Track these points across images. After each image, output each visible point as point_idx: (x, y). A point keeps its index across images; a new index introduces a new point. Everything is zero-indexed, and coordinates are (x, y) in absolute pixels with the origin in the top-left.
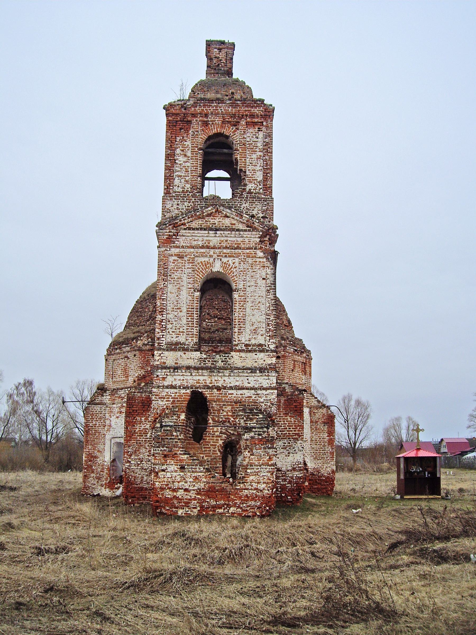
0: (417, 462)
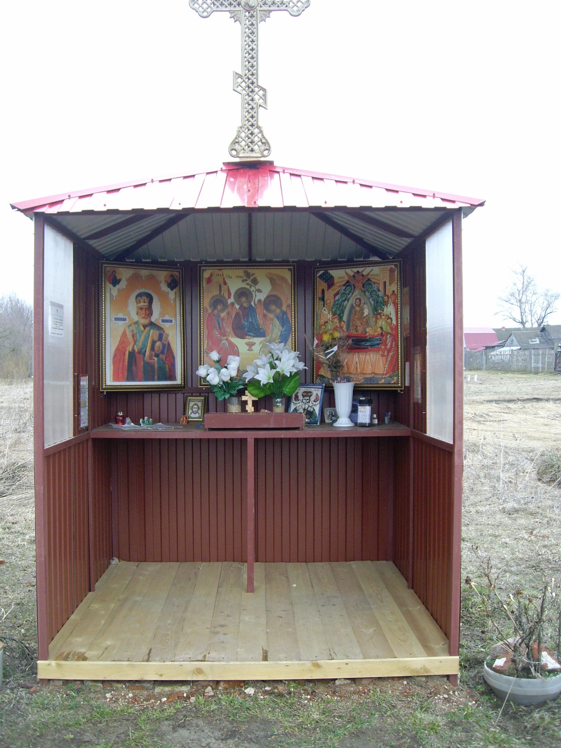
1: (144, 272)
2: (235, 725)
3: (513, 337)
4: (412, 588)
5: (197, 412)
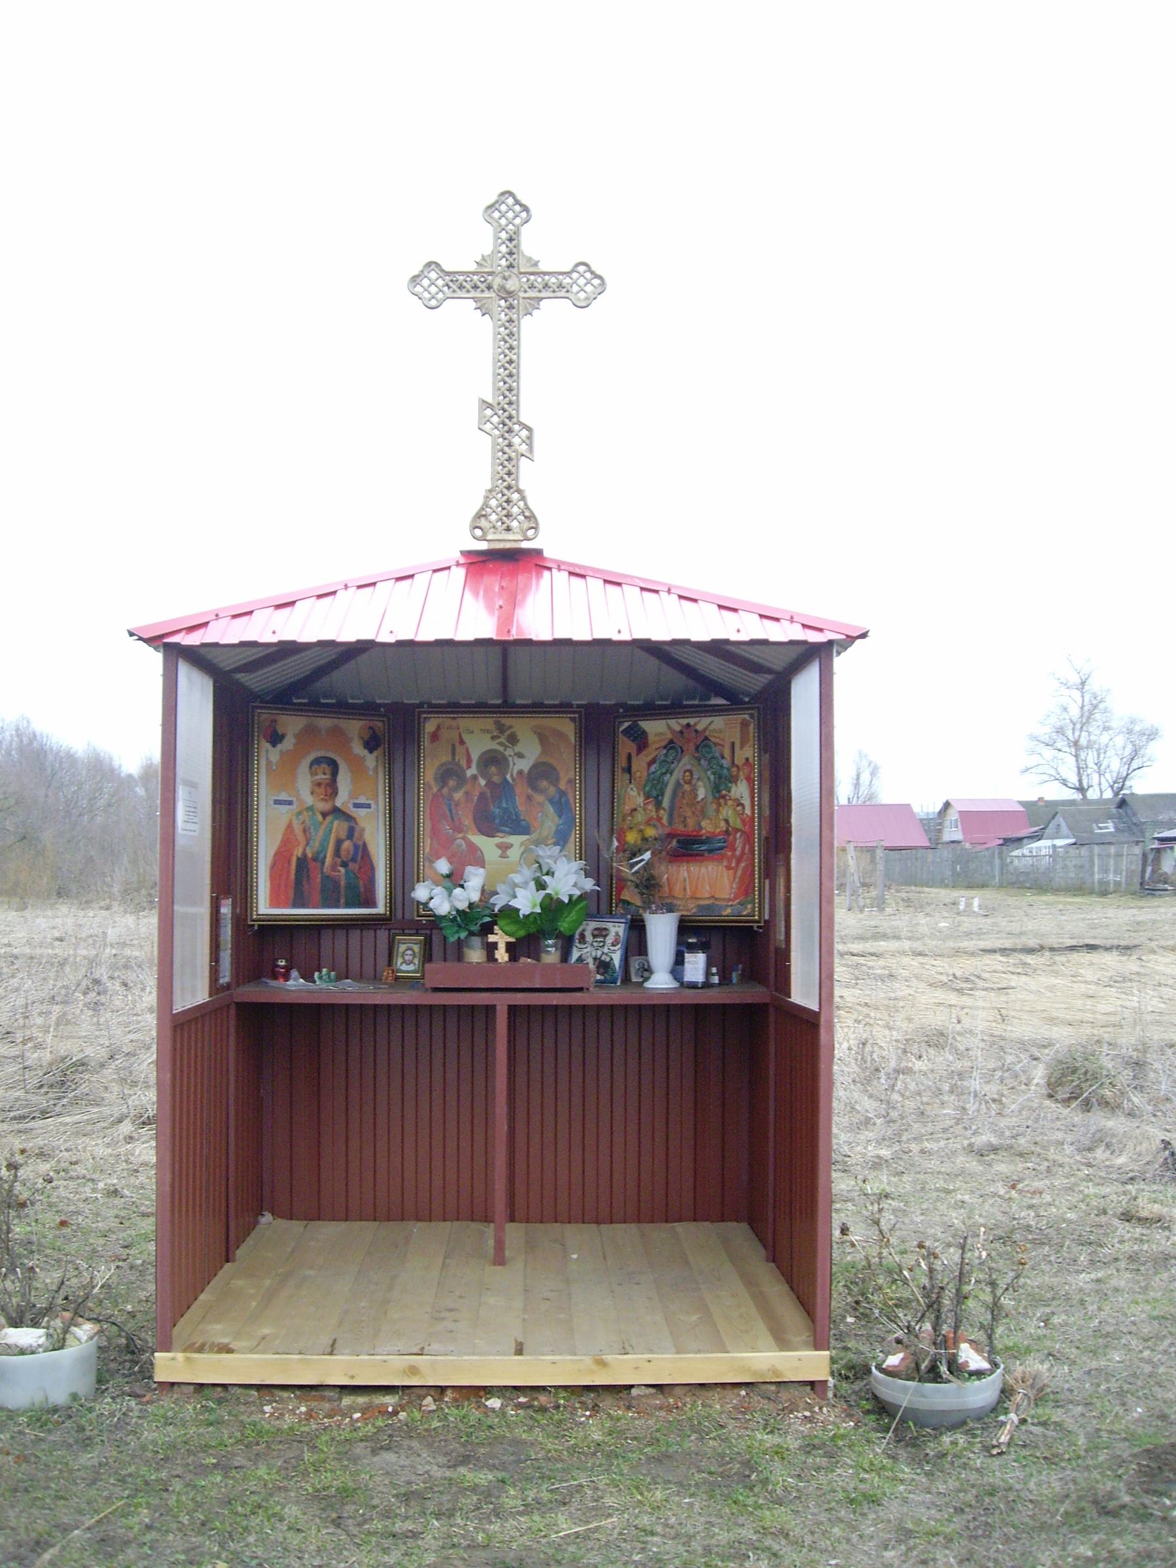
0: (542, 773)
1: (324, 723)
2: (469, 1447)
3: (1059, 819)
4: (774, 1261)
5: (411, 962)
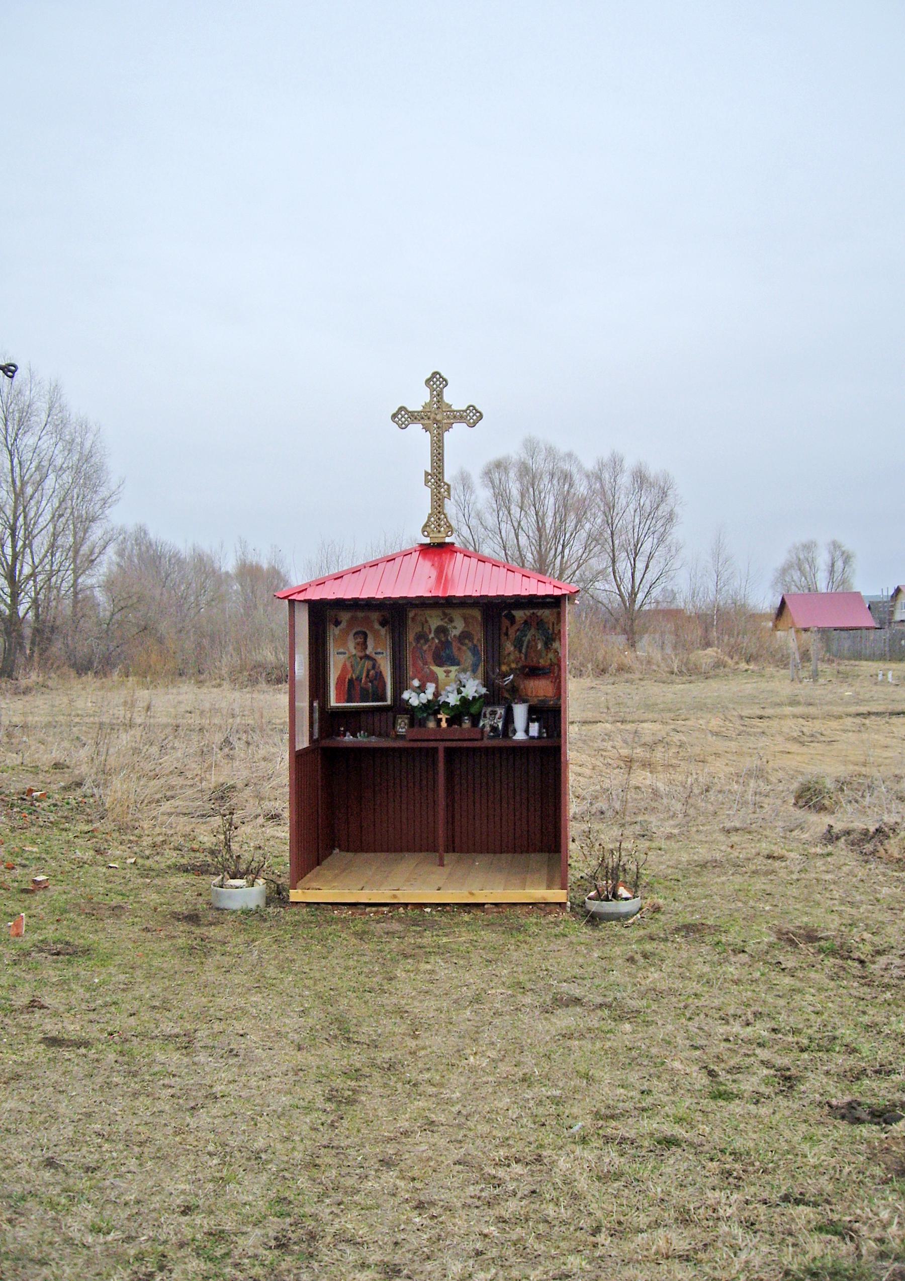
0: (465, 636)
1: (360, 615)
